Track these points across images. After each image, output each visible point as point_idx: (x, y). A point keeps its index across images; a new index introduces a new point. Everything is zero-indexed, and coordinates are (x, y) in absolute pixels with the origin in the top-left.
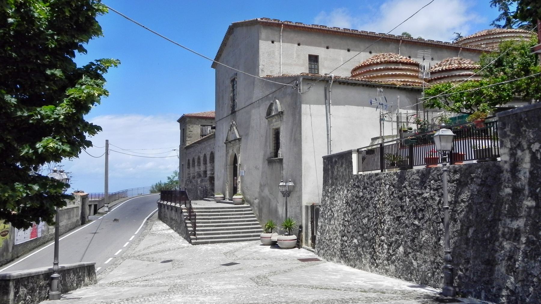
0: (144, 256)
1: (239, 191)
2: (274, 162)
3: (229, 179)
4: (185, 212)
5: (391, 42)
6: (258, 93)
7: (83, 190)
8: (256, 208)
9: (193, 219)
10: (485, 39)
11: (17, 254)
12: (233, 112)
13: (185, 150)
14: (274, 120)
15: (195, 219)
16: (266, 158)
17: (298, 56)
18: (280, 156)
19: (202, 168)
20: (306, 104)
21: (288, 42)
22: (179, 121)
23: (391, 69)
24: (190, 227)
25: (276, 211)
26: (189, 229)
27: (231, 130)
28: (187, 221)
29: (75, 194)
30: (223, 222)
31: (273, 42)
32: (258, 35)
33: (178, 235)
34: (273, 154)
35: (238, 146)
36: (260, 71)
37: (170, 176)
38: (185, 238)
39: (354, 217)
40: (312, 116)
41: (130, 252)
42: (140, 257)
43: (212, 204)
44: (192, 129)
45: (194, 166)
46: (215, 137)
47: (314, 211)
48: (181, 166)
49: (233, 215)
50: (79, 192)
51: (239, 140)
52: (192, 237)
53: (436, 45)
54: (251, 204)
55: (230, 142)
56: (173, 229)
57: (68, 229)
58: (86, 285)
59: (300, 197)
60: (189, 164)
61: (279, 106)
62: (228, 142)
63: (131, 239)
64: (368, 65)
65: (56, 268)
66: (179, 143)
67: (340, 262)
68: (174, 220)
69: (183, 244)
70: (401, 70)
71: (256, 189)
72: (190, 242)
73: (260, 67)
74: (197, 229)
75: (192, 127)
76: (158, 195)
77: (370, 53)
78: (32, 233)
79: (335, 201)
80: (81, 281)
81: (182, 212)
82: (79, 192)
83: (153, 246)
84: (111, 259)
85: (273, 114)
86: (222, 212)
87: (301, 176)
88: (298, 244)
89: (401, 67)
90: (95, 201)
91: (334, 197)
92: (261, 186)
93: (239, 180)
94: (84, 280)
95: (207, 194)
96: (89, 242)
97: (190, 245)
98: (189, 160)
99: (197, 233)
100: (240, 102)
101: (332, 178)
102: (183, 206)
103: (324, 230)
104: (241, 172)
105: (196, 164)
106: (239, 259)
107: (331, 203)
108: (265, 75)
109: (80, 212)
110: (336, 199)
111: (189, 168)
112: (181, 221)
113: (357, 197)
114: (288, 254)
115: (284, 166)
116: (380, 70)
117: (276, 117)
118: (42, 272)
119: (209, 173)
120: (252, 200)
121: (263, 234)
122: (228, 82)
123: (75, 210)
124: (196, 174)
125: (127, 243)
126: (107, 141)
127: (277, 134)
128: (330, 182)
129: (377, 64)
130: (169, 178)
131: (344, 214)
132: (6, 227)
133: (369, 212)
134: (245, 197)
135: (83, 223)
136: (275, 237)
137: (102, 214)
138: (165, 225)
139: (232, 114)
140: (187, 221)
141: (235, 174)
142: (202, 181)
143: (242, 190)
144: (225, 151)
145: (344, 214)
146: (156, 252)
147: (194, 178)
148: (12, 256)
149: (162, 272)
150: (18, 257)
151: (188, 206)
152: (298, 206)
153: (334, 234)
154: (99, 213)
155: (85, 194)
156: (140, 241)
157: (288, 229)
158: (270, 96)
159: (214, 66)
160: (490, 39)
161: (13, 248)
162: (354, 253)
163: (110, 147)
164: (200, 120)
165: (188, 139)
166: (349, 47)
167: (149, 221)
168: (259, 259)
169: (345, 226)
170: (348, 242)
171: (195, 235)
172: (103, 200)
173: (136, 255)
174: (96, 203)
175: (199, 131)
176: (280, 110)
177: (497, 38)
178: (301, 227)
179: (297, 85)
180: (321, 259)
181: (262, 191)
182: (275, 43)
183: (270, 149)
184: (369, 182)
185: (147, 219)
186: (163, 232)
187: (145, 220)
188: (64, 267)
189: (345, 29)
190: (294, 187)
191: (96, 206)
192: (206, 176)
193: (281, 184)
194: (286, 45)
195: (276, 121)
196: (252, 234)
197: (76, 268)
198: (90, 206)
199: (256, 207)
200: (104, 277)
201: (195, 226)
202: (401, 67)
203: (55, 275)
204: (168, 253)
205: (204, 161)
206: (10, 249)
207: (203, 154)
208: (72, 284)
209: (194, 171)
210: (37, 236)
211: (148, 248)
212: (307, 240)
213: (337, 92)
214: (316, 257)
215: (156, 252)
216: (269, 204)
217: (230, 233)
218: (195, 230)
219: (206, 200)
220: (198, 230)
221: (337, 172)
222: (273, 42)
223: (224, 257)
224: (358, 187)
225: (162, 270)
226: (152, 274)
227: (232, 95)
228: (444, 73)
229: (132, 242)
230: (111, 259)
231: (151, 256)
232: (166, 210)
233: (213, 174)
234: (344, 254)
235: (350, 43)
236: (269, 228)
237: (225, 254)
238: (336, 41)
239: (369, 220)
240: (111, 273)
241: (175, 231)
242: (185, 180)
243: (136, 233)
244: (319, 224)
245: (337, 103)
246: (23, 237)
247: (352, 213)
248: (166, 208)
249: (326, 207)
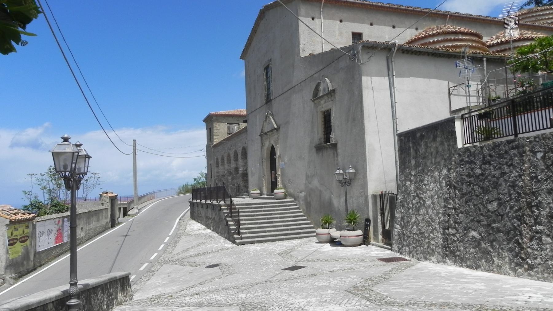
0: (184, 261)
1: (280, 185)
2: (325, 148)
3: (266, 173)
4: (224, 209)
5: (438, 17)
6: (299, 74)
7: (111, 191)
8: (302, 202)
9: (235, 216)
10: (526, 18)
11: (40, 262)
12: (268, 100)
13: (212, 149)
14: (322, 102)
15: (239, 216)
16: (314, 145)
17: (341, 33)
18: (333, 140)
19: (233, 165)
20: (367, 76)
21: (330, 19)
22: (204, 121)
23: (451, 40)
24: (232, 225)
25: (330, 203)
26: (231, 227)
27: (266, 121)
28: (228, 219)
29: (104, 195)
30: (268, 219)
31: (313, 19)
32: (297, 10)
33: (217, 235)
34: (323, 140)
35: (276, 136)
36: (301, 51)
37: (196, 177)
38: (226, 238)
39: (466, 202)
40: (374, 89)
41: (167, 256)
42: (179, 262)
43: (247, 200)
44: (218, 128)
45: (223, 163)
46: (247, 131)
47: (388, 202)
48: (209, 166)
49: (277, 210)
50: (107, 193)
51: (278, 129)
52: (236, 236)
53: (484, 20)
54: (296, 198)
55: (266, 134)
56: (209, 228)
57: (97, 232)
58: (120, 304)
59: (365, 186)
60: (217, 163)
61: (328, 84)
62: (263, 134)
63: (166, 241)
64: (423, 38)
65: (74, 290)
66: (205, 142)
67: (444, 262)
68: (211, 219)
69: (226, 245)
70: (461, 40)
71: (302, 181)
72: (234, 242)
73: (301, 46)
74: (241, 227)
75: (219, 125)
76: (190, 195)
77: (417, 29)
78: (57, 238)
79: (425, 185)
80: (113, 299)
81: (221, 209)
82: (107, 193)
83: (192, 248)
84: (146, 265)
85: (321, 95)
86: (265, 207)
87: (365, 161)
88: (365, 241)
89: (460, 37)
90: (124, 204)
91: (422, 181)
92: (307, 177)
93: (279, 173)
94: (116, 298)
95: (243, 190)
96: (120, 246)
97: (235, 245)
98: (217, 159)
99: (241, 231)
100: (275, 90)
101: (415, 158)
102: (222, 203)
103: (408, 222)
104: (279, 164)
105: (226, 162)
106: (301, 261)
107: (417, 188)
108: (307, 54)
109: (109, 213)
110: (426, 182)
111: (217, 166)
112: (220, 219)
113: (469, 176)
114: (359, 252)
115: (339, 151)
116: (438, 42)
117: (326, 98)
118: (50, 299)
119: (241, 169)
120: (296, 194)
121: (319, 231)
122: (261, 71)
123: (104, 212)
124: (226, 172)
125: (162, 246)
126: (134, 141)
127: (327, 117)
128: (413, 162)
129: (434, 35)
130: (195, 180)
131: (446, 200)
132: (25, 232)
133: (499, 194)
134: (287, 191)
135: (113, 225)
136: (335, 233)
137: (132, 216)
138: (199, 224)
139: (267, 103)
140: (228, 219)
141: (273, 166)
142: (233, 178)
143: (283, 184)
144: (260, 145)
145: (446, 200)
146: (197, 255)
147: (224, 176)
148: (35, 265)
149: (211, 280)
150: (41, 266)
151: (228, 202)
152: (362, 196)
153: (429, 226)
154: (129, 215)
155: (114, 194)
156: (176, 242)
157: (352, 222)
158: (316, 75)
159: (242, 57)
160: (533, 16)
161: (35, 256)
162: (472, 250)
163: (138, 147)
164: (227, 118)
165: (215, 137)
166: (395, 24)
167: (182, 221)
168: (327, 261)
169: (449, 215)
170: (458, 235)
171: (239, 234)
172: (132, 202)
173: (174, 259)
174: (125, 206)
175: (226, 129)
176: (330, 88)
177: (540, 15)
178: (368, 220)
179: (354, 55)
180: (407, 257)
181: (310, 183)
182: (315, 19)
183: (319, 134)
184: (493, 154)
185: (180, 220)
186: (200, 232)
187: (178, 220)
188: (87, 285)
189: (389, 4)
190: (355, 174)
191: (125, 209)
192: (238, 173)
193: (338, 172)
194: (328, 22)
195: (325, 102)
196: (301, 231)
197: (106, 284)
198: (120, 208)
199: (303, 201)
200: (141, 292)
201: (238, 224)
202: (460, 37)
203: (73, 302)
204: (211, 255)
205: (234, 158)
206: (32, 257)
207: (234, 150)
208: (101, 306)
209: (224, 169)
210: (62, 241)
211: (187, 250)
212: (376, 236)
213: (400, 63)
214: (398, 255)
215: (197, 255)
216: (320, 196)
217: (277, 231)
218: (239, 229)
219: (240, 198)
220: (242, 229)
221: (426, 149)
222: (313, 19)
223: (280, 259)
224: (471, 162)
225: (209, 277)
226: (200, 284)
227: (266, 83)
228: (504, 46)
229: (167, 245)
230: (146, 265)
231: (192, 260)
232: (201, 209)
233: (246, 170)
234: (452, 252)
235: (395, 19)
236: (325, 223)
237: (281, 254)
238: (380, 17)
239: (500, 205)
240: (149, 283)
241: (213, 231)
242: (213, 179)
243: (170, 234)
244: (397, 215)
245: (400, 75)
246: (46, 243)
247: (461, 198)
248: (200, 206)
249: (409, 194)
